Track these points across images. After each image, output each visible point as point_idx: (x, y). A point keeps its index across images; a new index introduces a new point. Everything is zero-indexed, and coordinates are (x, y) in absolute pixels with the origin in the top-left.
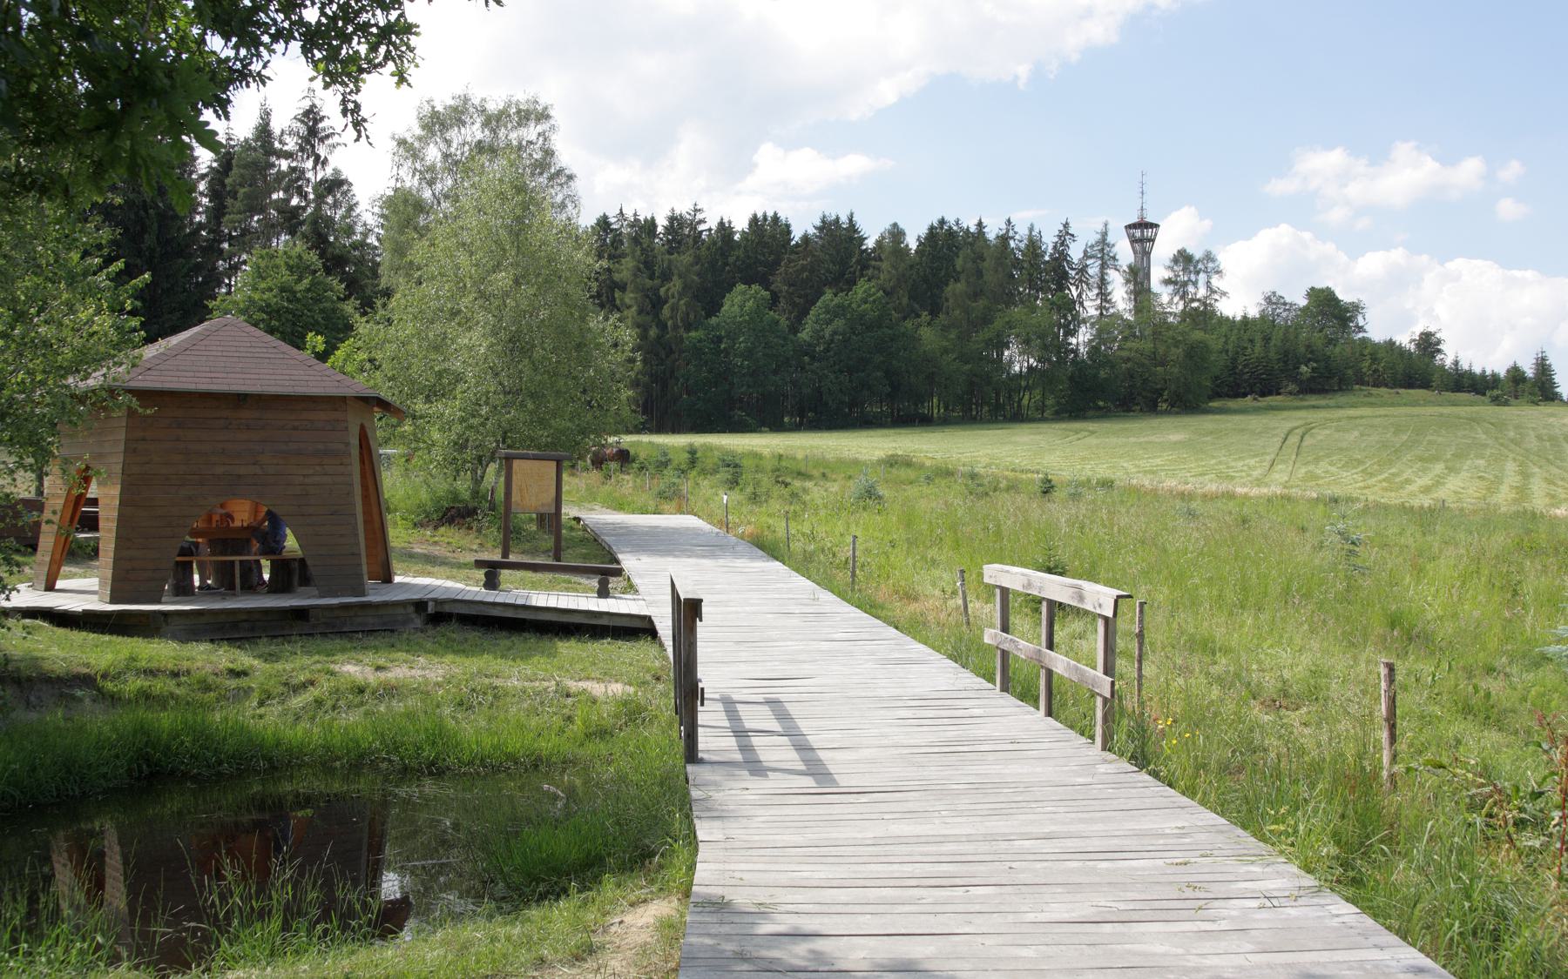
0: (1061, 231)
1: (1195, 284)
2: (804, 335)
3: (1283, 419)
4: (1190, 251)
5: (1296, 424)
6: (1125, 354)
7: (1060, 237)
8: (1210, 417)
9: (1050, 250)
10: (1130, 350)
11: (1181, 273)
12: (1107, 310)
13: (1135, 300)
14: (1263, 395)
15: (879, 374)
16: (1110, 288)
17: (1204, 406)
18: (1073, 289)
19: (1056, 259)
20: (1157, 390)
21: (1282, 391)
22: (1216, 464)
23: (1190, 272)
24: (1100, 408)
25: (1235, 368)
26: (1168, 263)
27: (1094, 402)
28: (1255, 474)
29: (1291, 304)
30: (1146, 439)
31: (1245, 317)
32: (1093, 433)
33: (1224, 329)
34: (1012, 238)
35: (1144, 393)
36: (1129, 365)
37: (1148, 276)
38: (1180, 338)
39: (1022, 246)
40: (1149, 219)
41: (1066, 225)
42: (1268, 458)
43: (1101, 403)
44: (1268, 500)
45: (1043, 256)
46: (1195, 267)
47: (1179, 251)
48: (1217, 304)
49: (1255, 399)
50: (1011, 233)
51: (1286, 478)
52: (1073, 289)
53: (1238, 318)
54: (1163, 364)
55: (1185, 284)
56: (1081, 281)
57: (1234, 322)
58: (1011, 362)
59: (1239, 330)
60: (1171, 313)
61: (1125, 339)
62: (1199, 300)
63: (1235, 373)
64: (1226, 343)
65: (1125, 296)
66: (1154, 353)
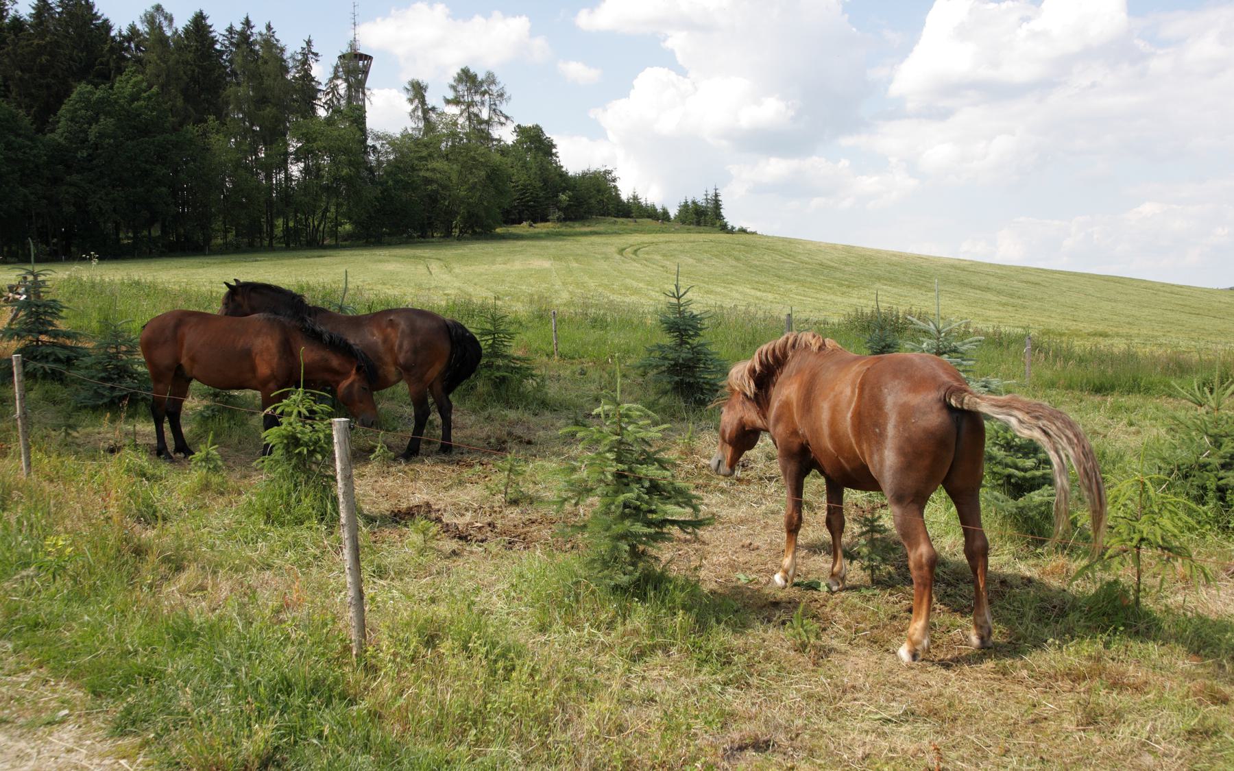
2: (59, 134)
15: (163, 189)
40: (362, 51)
41: (309, 43)
49: (531, 226)
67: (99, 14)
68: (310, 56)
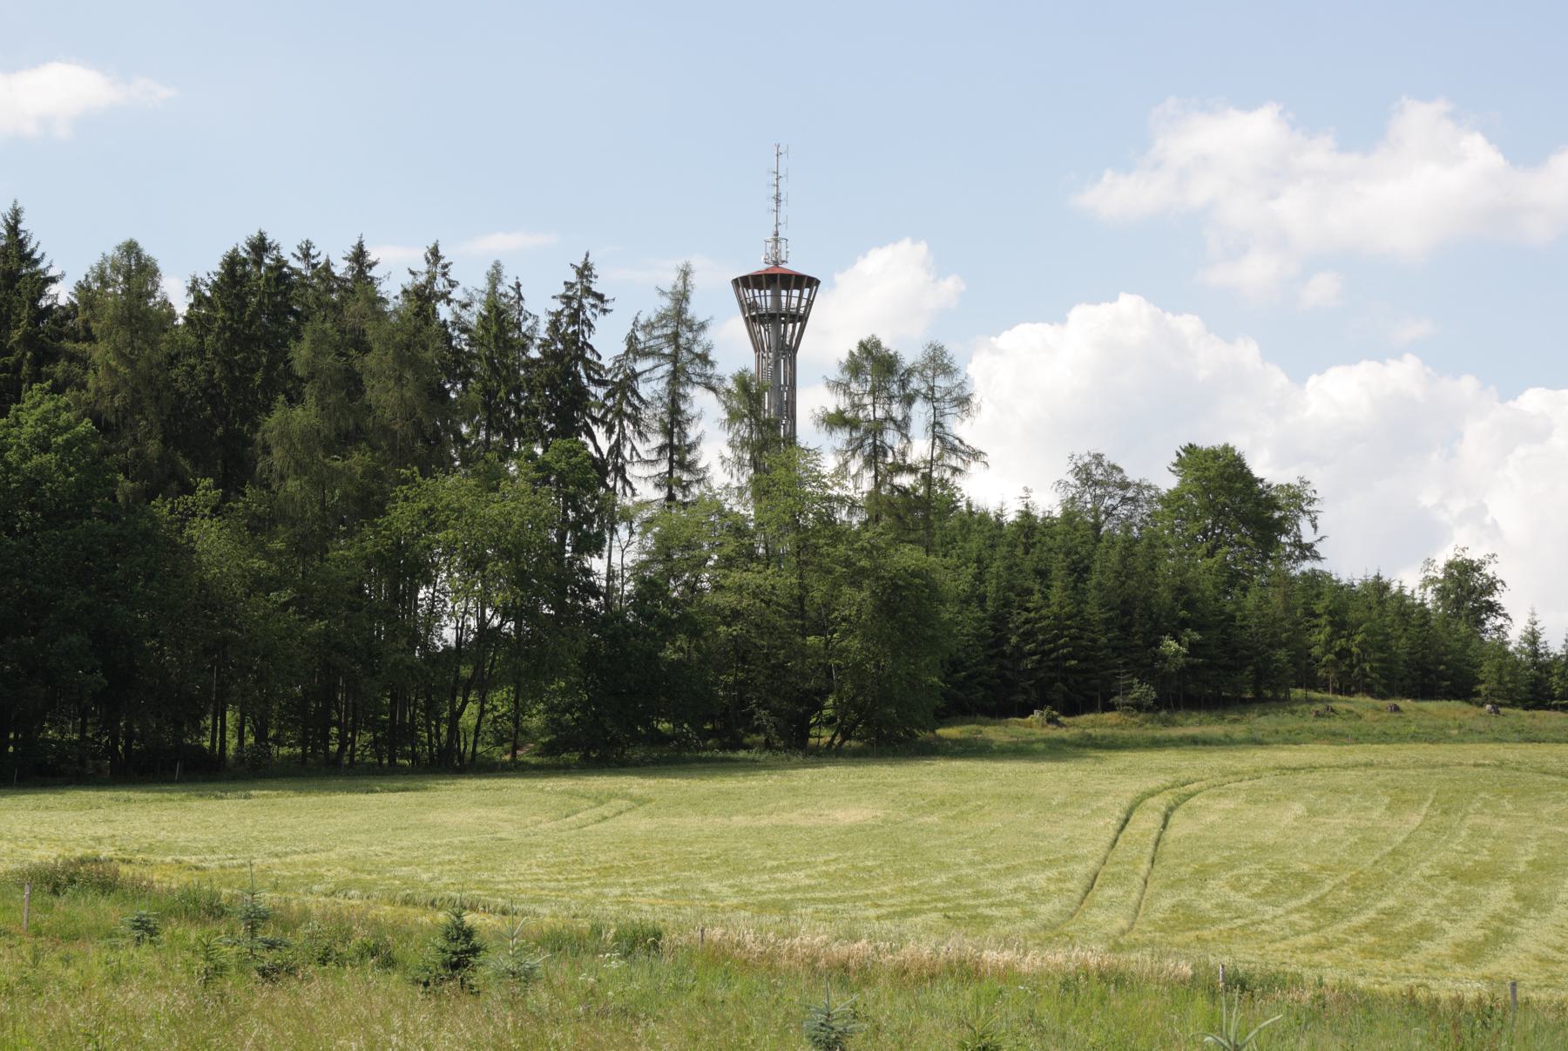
41: (585, 271)
49: (1052, 720)
67: (36, 256)
68: (588, 301)
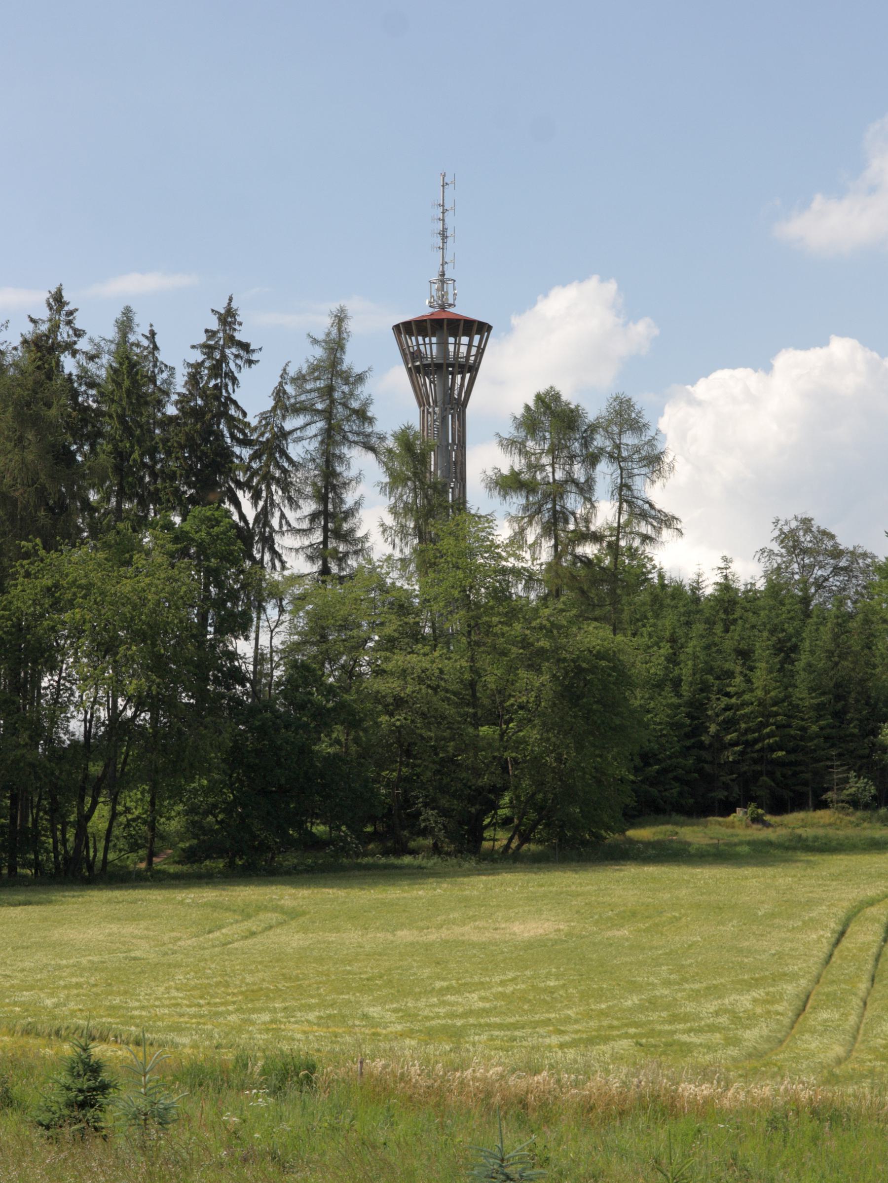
0: (211, 334)
1: (586, 490)
3: (835, 877)
4: (569, 396)
5: (871, 892)
6: (388, 686)
7: (208, 349)
8: (631, 871)
9: (180, 384)
10: (404, 673)
11: (546, 460)
12: (341, 559)
13: (420, 532)
14: (779, 807)
16: (349, 498)
17: (612, 837)
18: (244, 497)
19: (197, 413)
20: (479, 791)
21: (830, 795)
22: (641, 1008)
23: (572, 457)
24: (315, 844)
25: (698, 730)
26: (509, 430)
27: (300, 826)
28: (751, 1036)
29: (854, 555)
30: (444, 933)
31: (726, 587)
32: (293, 914)
33: (668, 621)
34: (70, 347)
35: (444, 802)
36: (399, 719)
37: (457, 470)
38: (544, 643)
39: (100, 370)
40: (463, 309)
41: (228, 318)
42: (790, 989)
43: (320, 829)
44: (773, 1123)
45: (160, 404)
46: (586, 442)
47: (539, 398)
48: (649, 550)
50: (64, 333)
51: (839, 1050)
52: (244, 497)
53: (709, 590)
54: (494, 718)
55: (557, 491)
56: (268, 478)
57: (696, 600)
58: (58, 707)
59: (710, 623)
60: (517, 573)
61: (389, 644)
62: (596, 538)
63: (701, 746)
64: (673, 660)
65: (390, 520)
66: (472, 685)
